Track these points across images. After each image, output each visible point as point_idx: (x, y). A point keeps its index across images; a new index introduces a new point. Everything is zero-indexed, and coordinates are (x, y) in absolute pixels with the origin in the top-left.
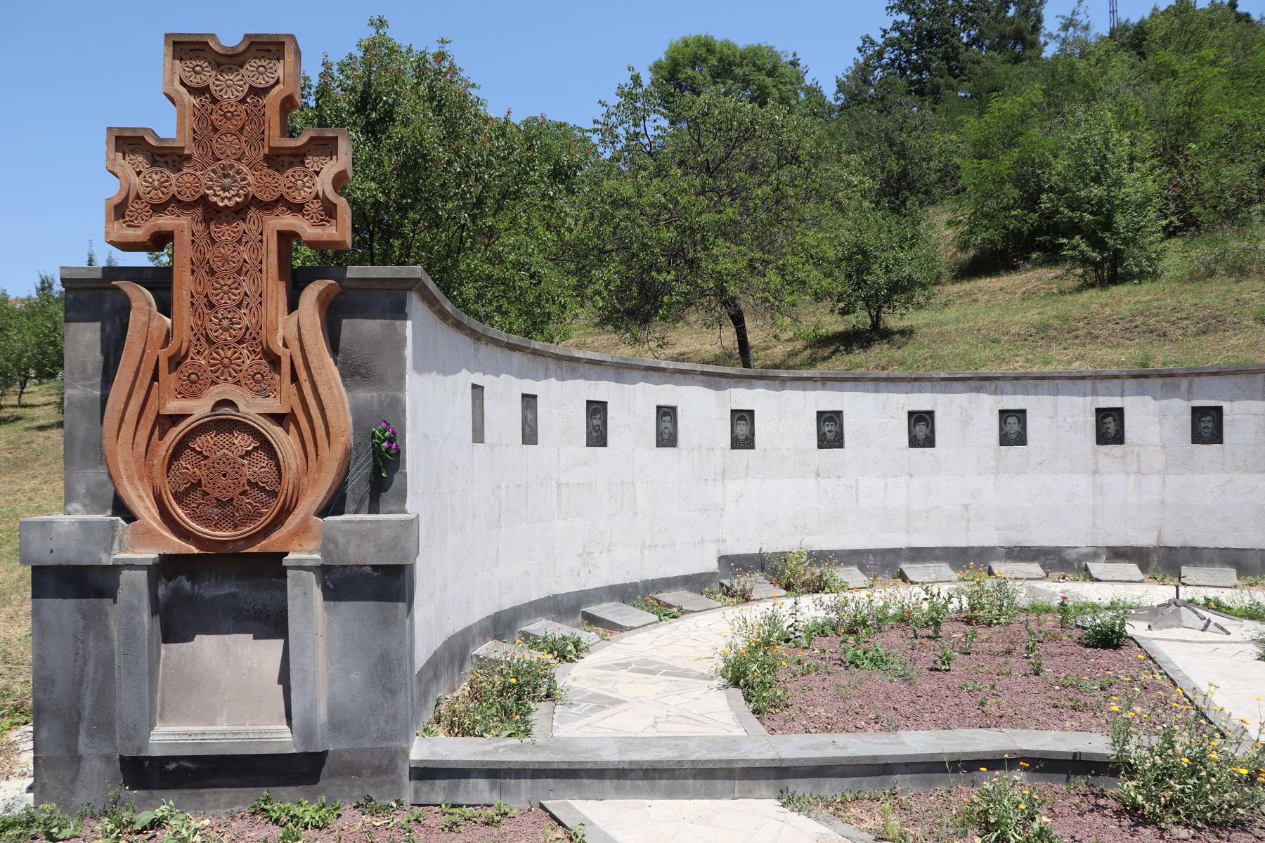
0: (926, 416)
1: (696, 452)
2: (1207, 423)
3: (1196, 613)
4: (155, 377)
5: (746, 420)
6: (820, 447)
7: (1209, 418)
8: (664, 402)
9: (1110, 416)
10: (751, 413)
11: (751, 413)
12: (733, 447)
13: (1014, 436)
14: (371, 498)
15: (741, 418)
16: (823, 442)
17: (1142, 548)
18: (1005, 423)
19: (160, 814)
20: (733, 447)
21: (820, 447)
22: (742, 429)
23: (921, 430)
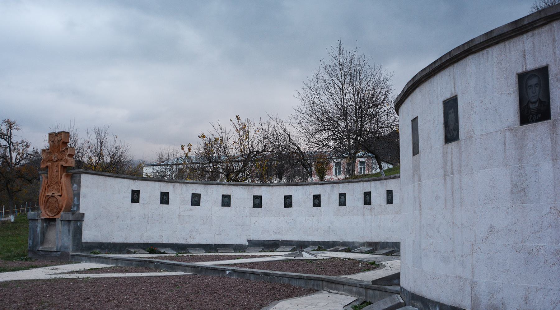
0: (259, 197)
1: (238, 208)
2: (196, 199)
3: (329, 257)
4: (45, 190)
5: (259, 199)
6: (285, 207)
7: (227, 198)
8: (225, 193)
9: (227, 197)
10: (261, 197)
11: (261, 197)
12: (253, 207)
13: (343, 203)
14: (390, 252)
15: (257, 198)
16: (286, 206)
17: (376, 242)
18: (341, 197)
19: (6, 254)
20: (253, 207)
21: (285, 207)
22: (317, 201)
23: (257, 202)
